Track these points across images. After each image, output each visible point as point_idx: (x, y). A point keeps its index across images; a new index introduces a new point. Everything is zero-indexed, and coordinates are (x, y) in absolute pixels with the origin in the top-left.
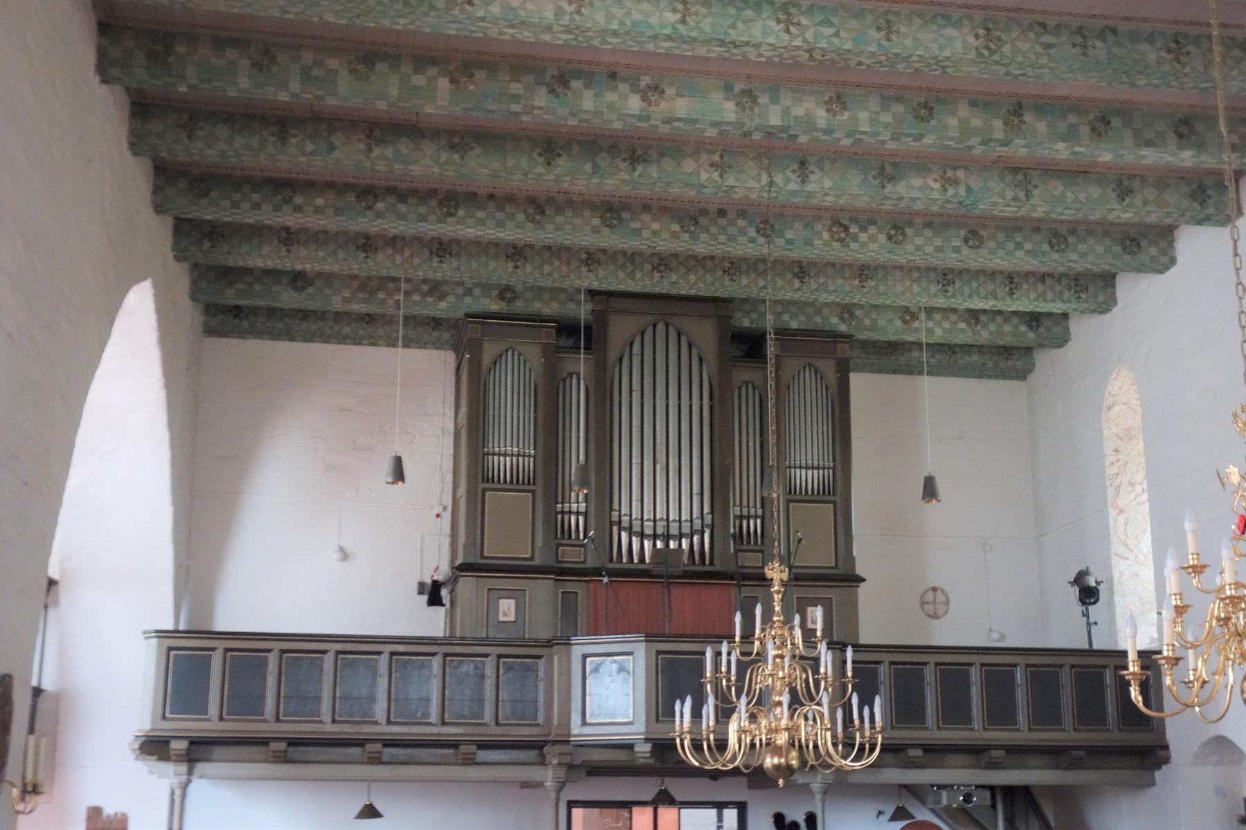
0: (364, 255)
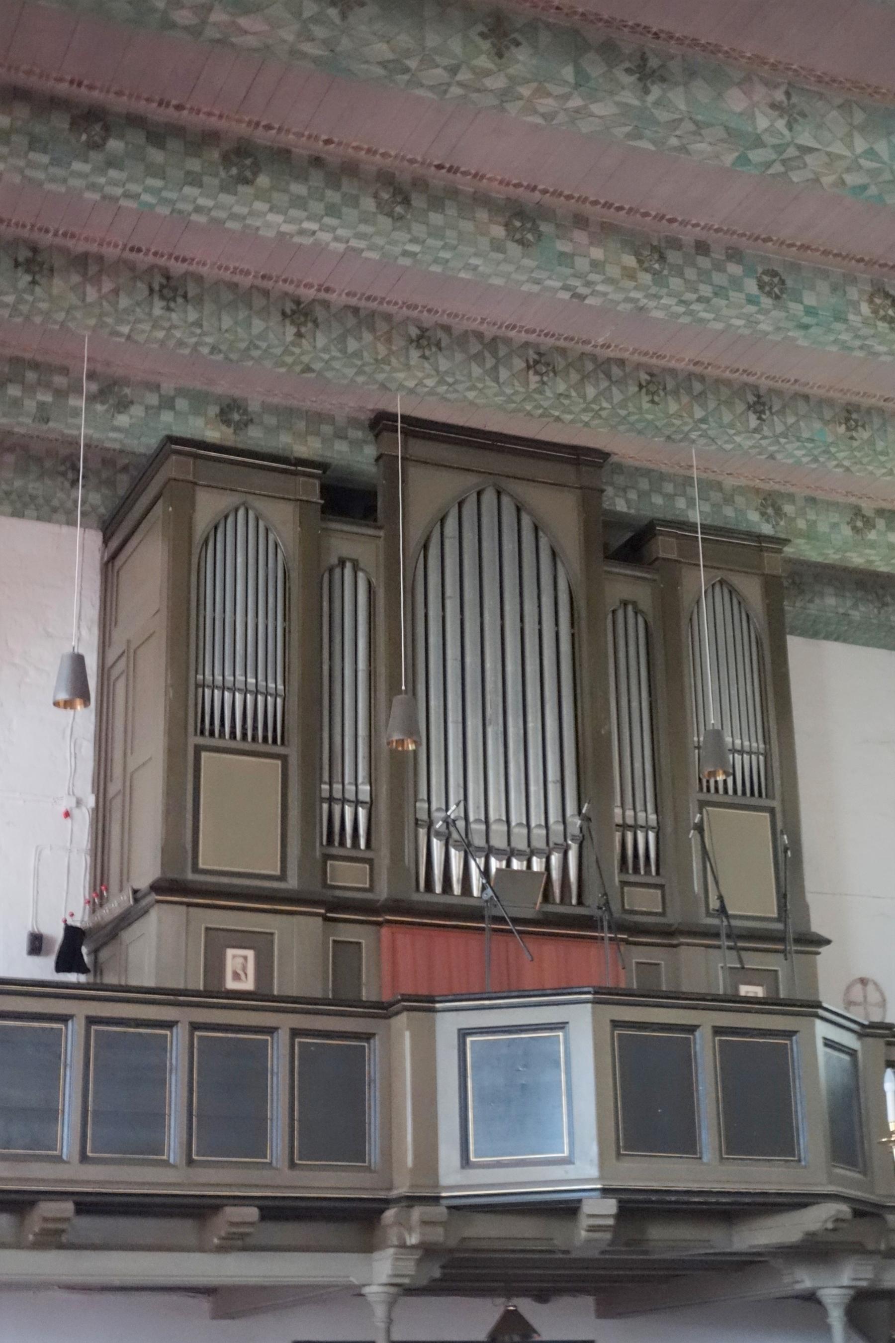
0: (29, 278)
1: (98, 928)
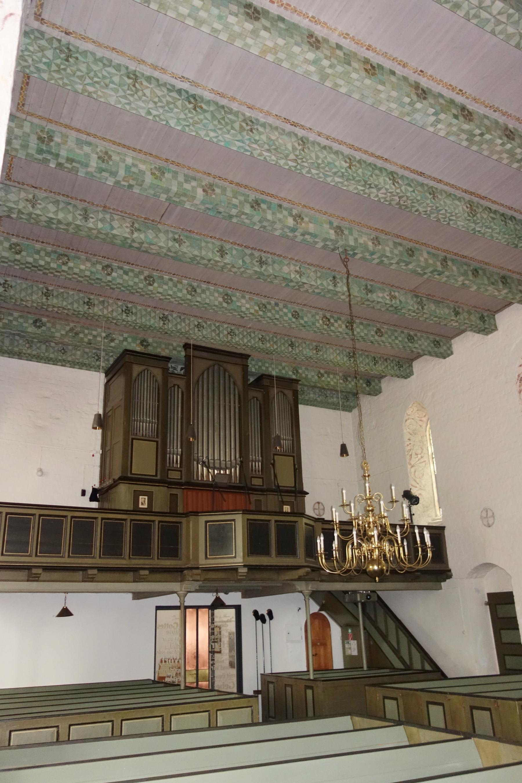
1: (102, 489)
